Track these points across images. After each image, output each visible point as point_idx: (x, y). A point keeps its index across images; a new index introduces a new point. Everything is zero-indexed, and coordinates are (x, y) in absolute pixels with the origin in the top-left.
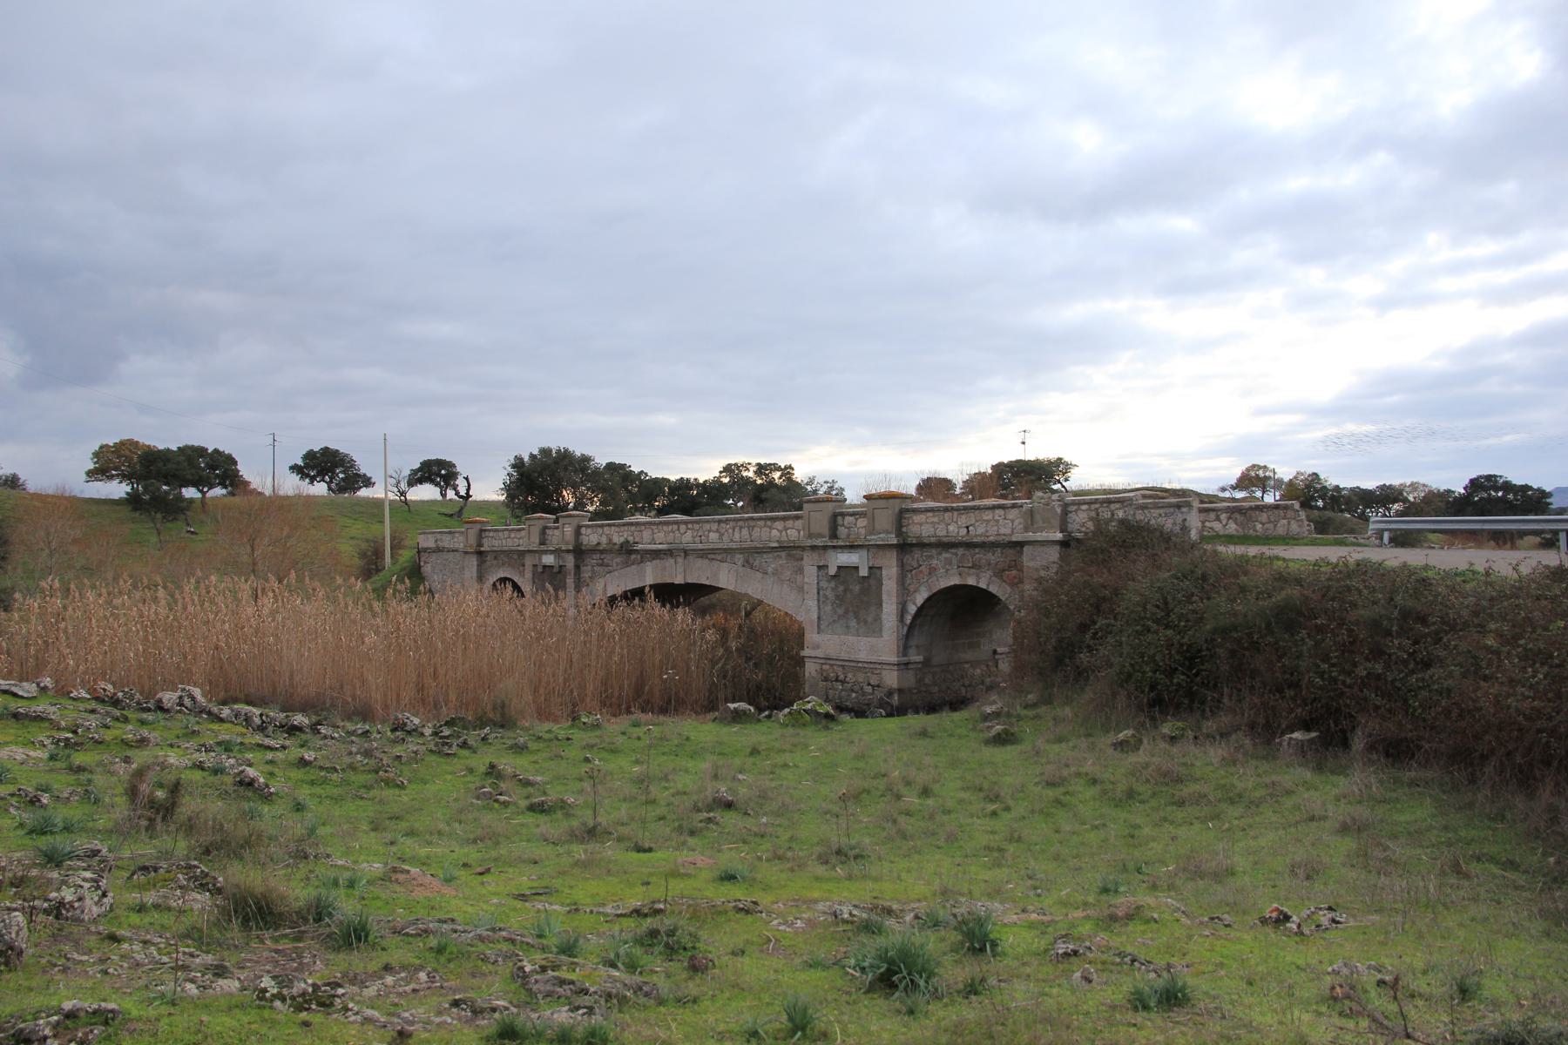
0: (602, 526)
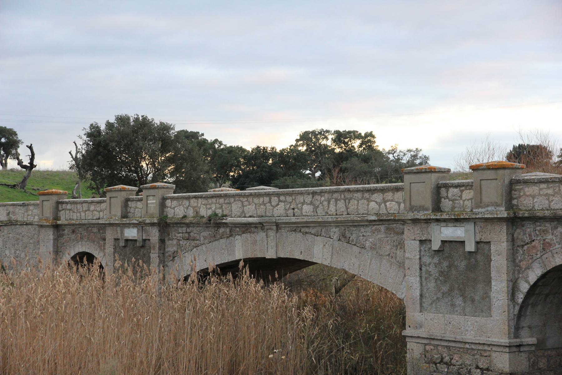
0: (188, 198)
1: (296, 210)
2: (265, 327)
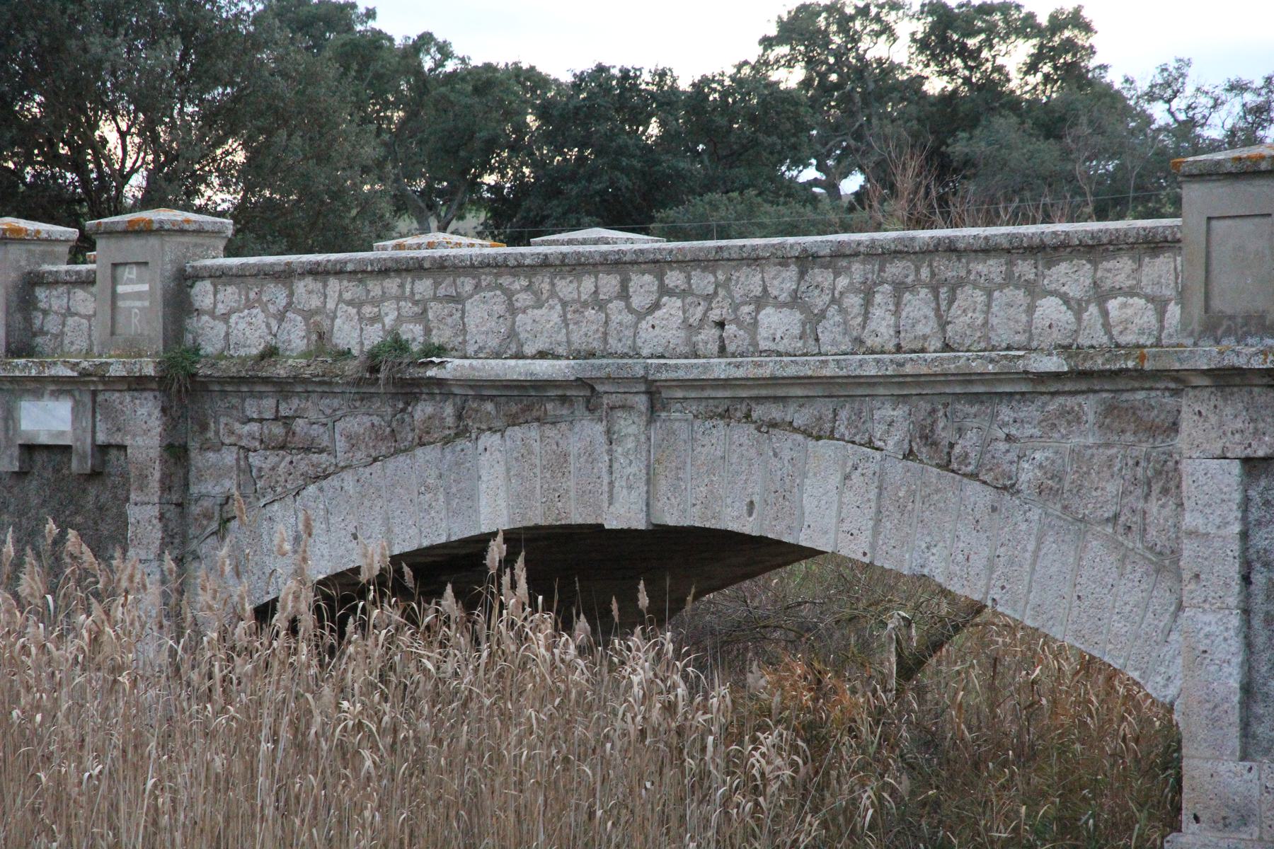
0: (286, 276)
1: (731, 329)
2: (591, 815)
